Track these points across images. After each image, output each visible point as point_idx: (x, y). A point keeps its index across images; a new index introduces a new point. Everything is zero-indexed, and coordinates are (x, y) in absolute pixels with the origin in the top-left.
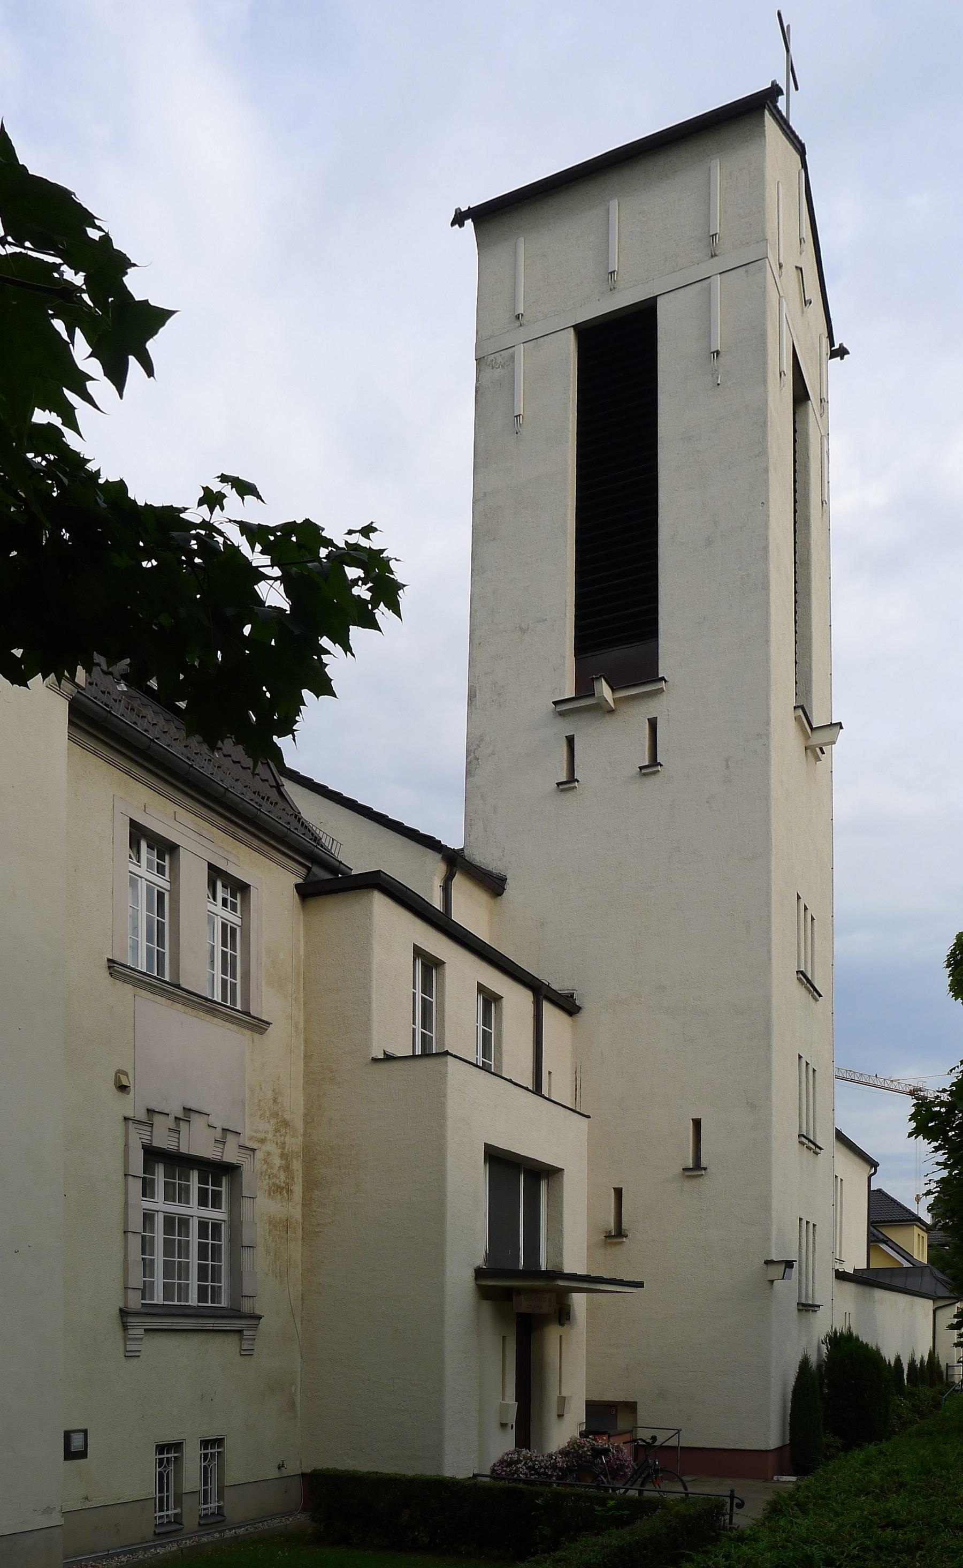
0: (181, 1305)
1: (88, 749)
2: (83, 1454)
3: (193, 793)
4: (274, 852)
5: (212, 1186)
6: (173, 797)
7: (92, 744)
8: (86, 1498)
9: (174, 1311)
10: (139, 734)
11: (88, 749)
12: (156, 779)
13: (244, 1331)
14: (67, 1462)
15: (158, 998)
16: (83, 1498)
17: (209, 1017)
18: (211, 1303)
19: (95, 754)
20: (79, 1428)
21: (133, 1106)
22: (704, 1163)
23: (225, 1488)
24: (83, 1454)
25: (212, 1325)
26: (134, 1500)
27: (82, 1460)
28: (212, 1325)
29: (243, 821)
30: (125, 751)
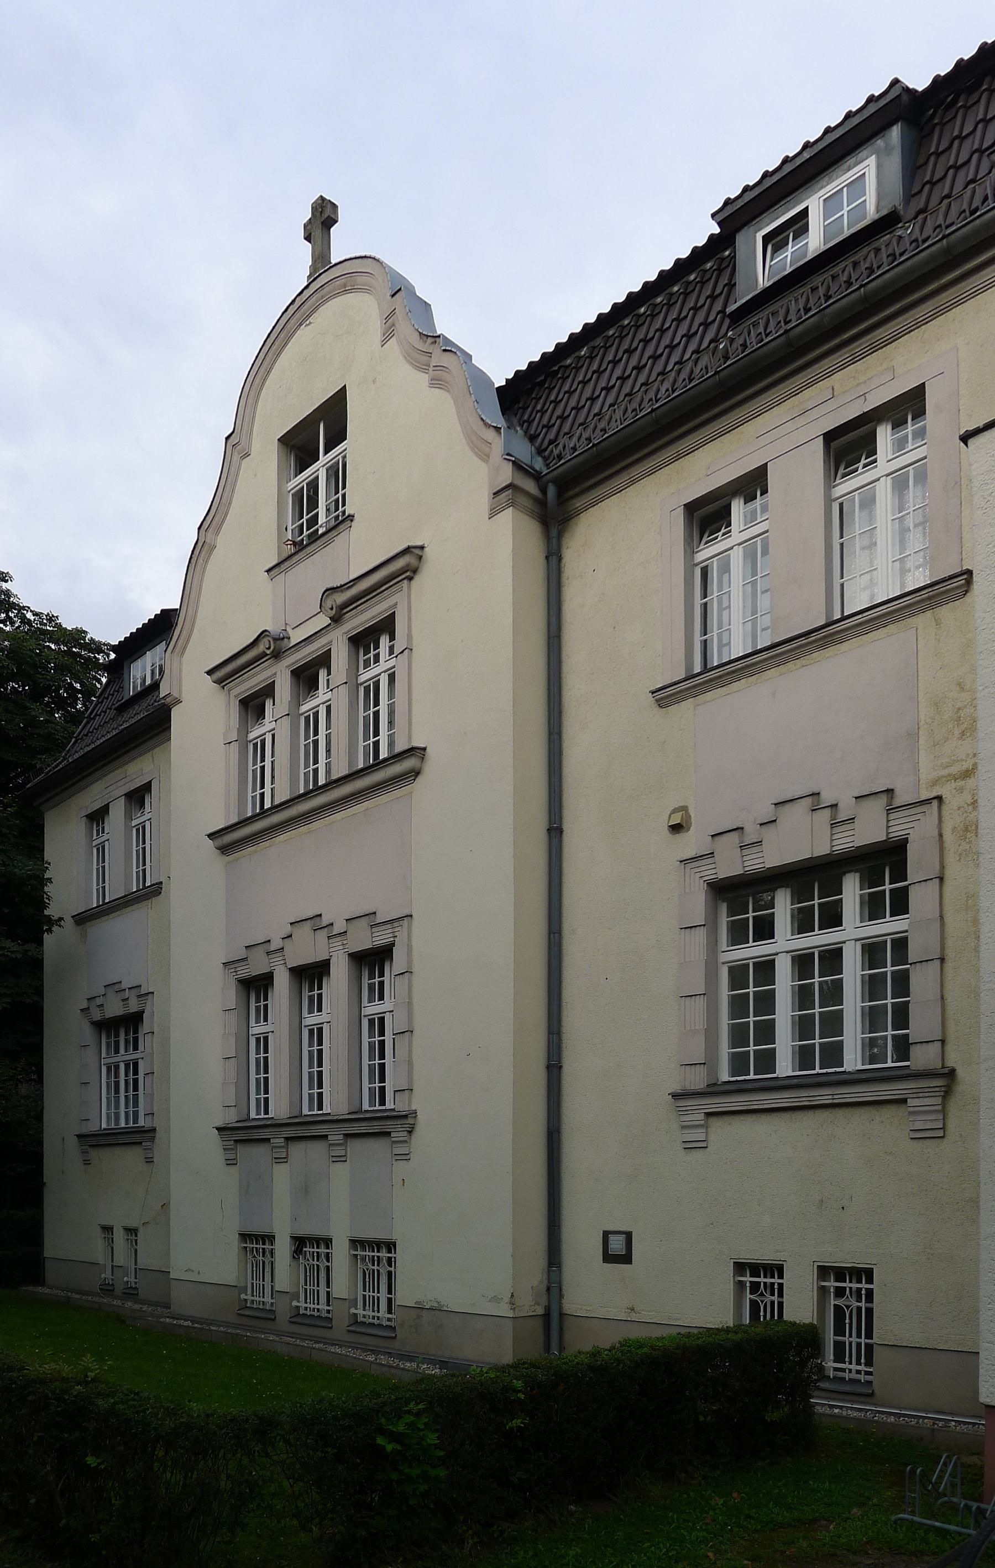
0: (737, 1081)
1: (736, 425)
2: (626, 1258)
3: (863, 326)
4: (970, 280)
5: (748, 913)
6: (736, 422)
7: (624, 478)
8: (633, 1309)
9: (750, 1086)
10: (635, 424)
11: (736, 425)
12: (750, 404)
13: (392, 1133)
14: (607, 1264)
15: (709, 696)
16: (628, 1308)
17: (831, 651)
18: (380, 1105)
19: (633, 482)
20: (622, 1230)
21: (691, 843)
22: (970, 442)
23: (172, 1281)
24: (626, 1258)
25: (830, 1097)
26: (698, 1326)
27: (626, 1265)
28: (830, 1097)
29: (718, 404)
30: (655, 445)
